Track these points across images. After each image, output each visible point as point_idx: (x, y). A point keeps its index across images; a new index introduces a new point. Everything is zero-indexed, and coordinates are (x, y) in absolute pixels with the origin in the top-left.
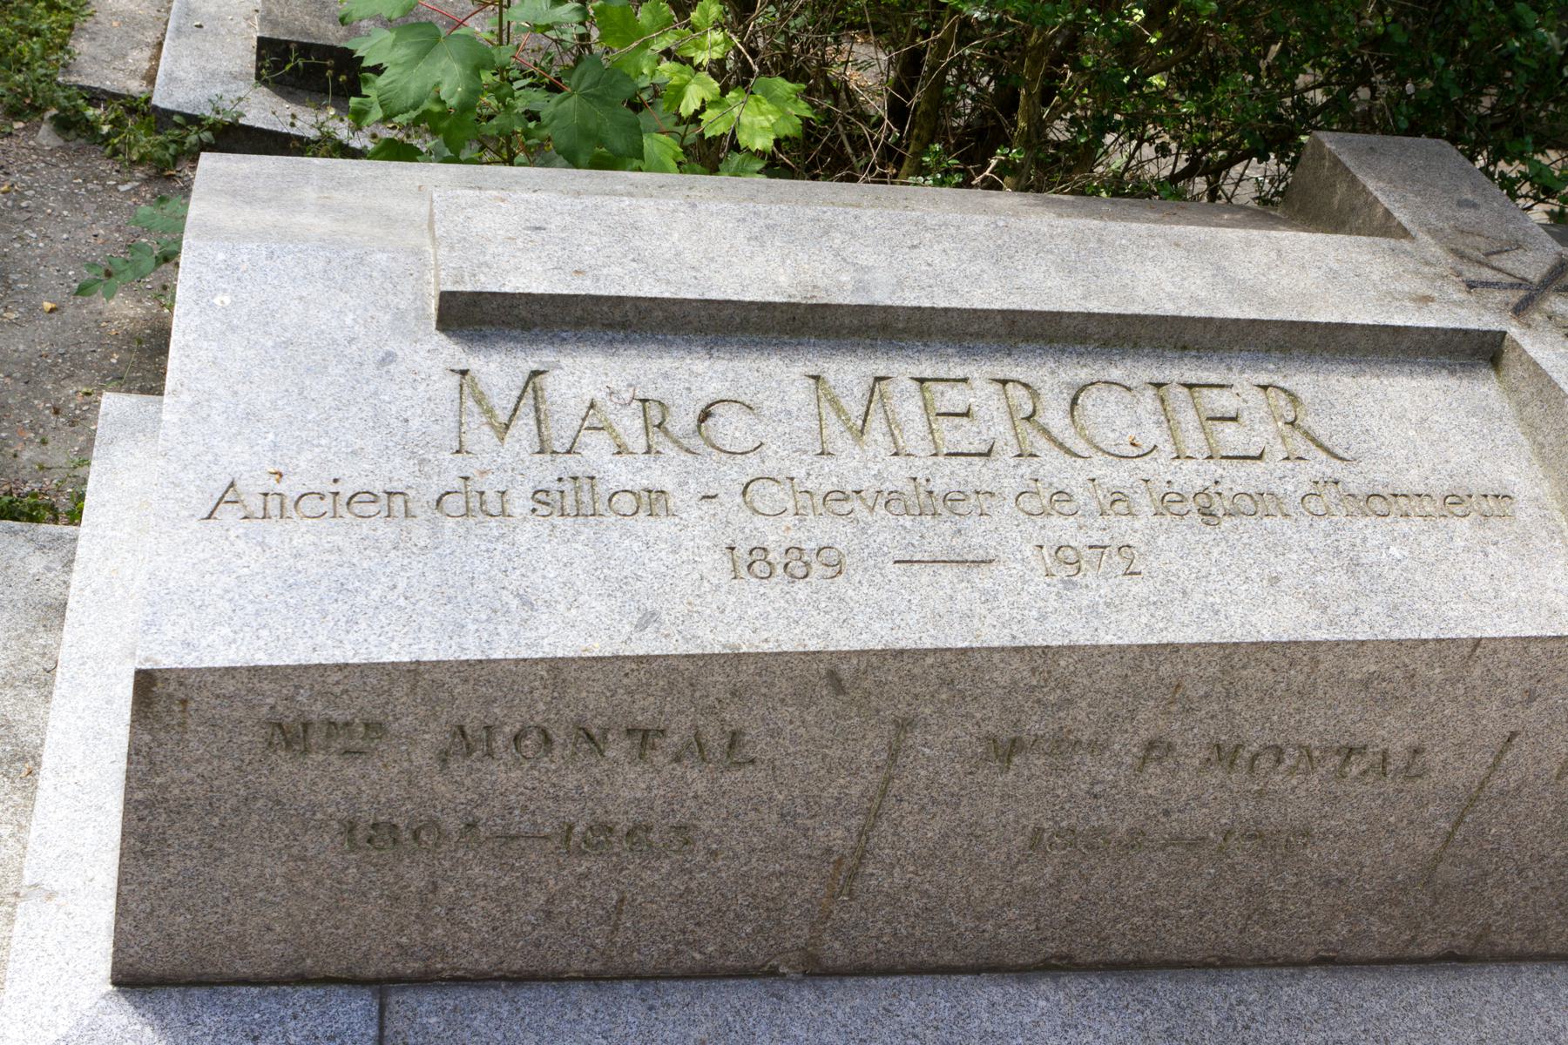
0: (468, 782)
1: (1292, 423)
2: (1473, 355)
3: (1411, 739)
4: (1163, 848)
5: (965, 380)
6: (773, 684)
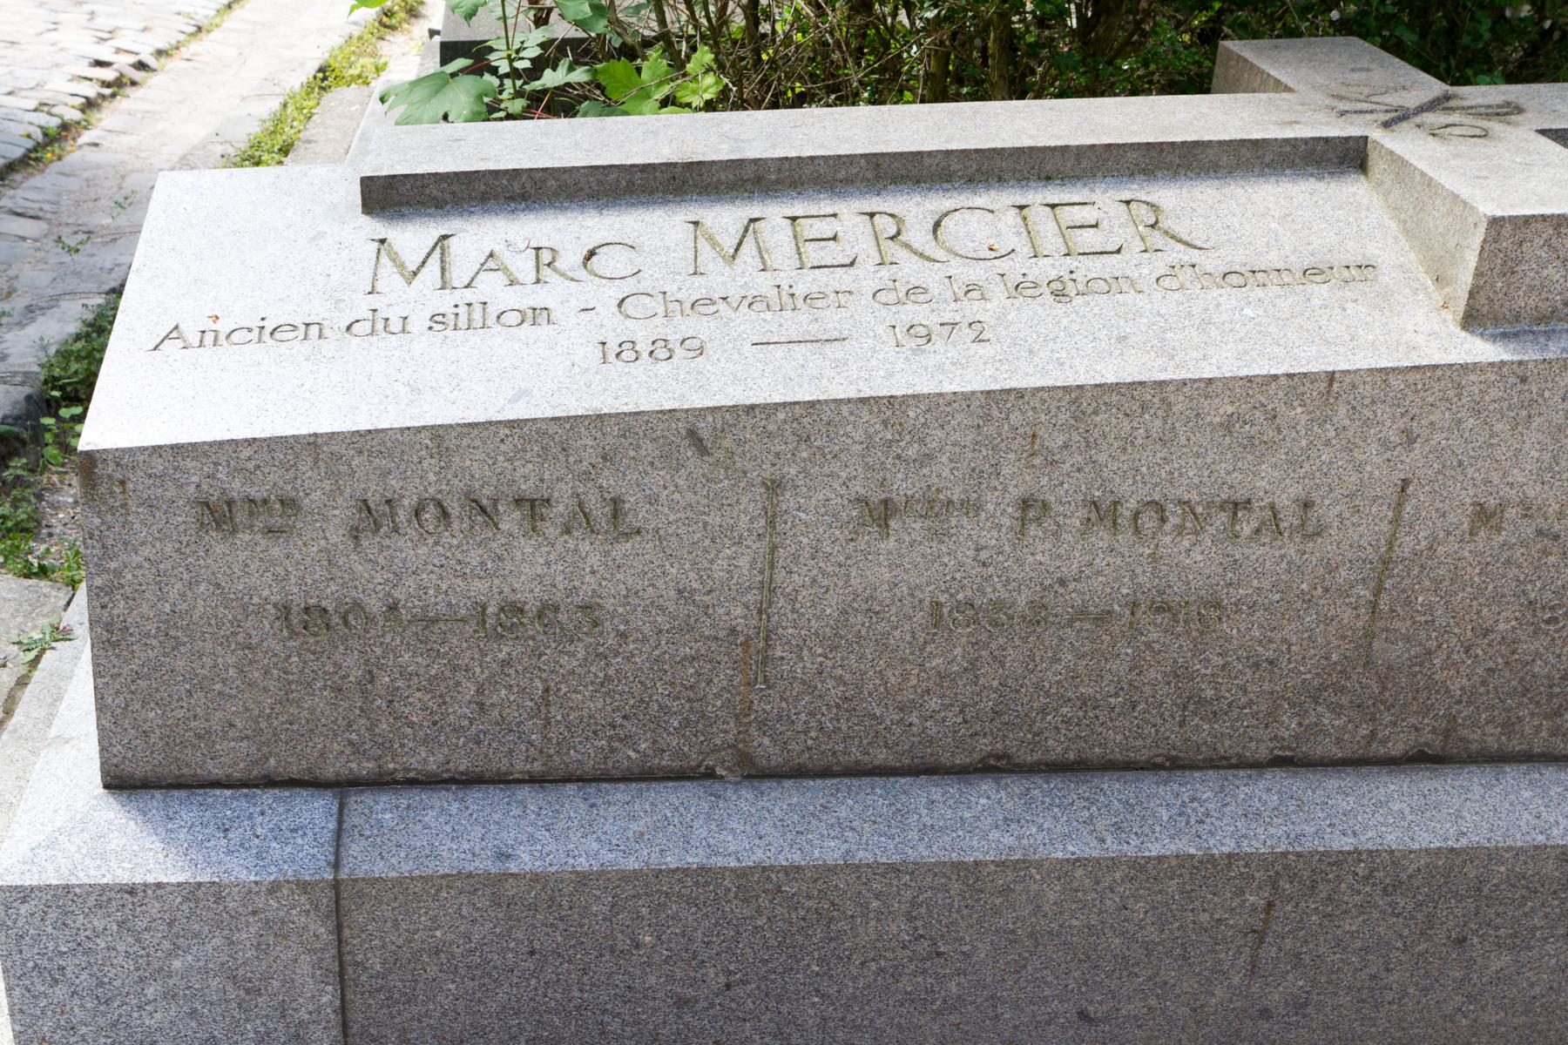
0: (381, 560)
1: (1152, 226)
2: (1341, 163)
3: (1295, 490)
4: (1070, 624)
5: (835, 215)
6: (639, 447)
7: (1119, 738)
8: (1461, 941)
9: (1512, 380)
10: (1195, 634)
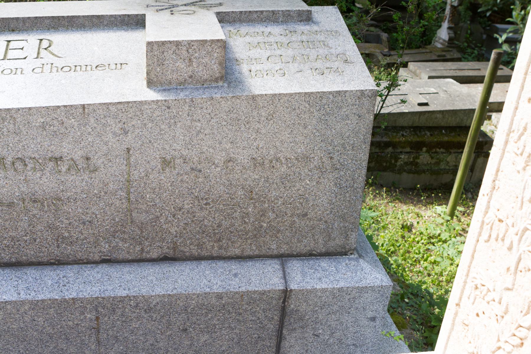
7: (32, 253)
8: (185, 330)
9: (164, 108)
10: (53, 211)
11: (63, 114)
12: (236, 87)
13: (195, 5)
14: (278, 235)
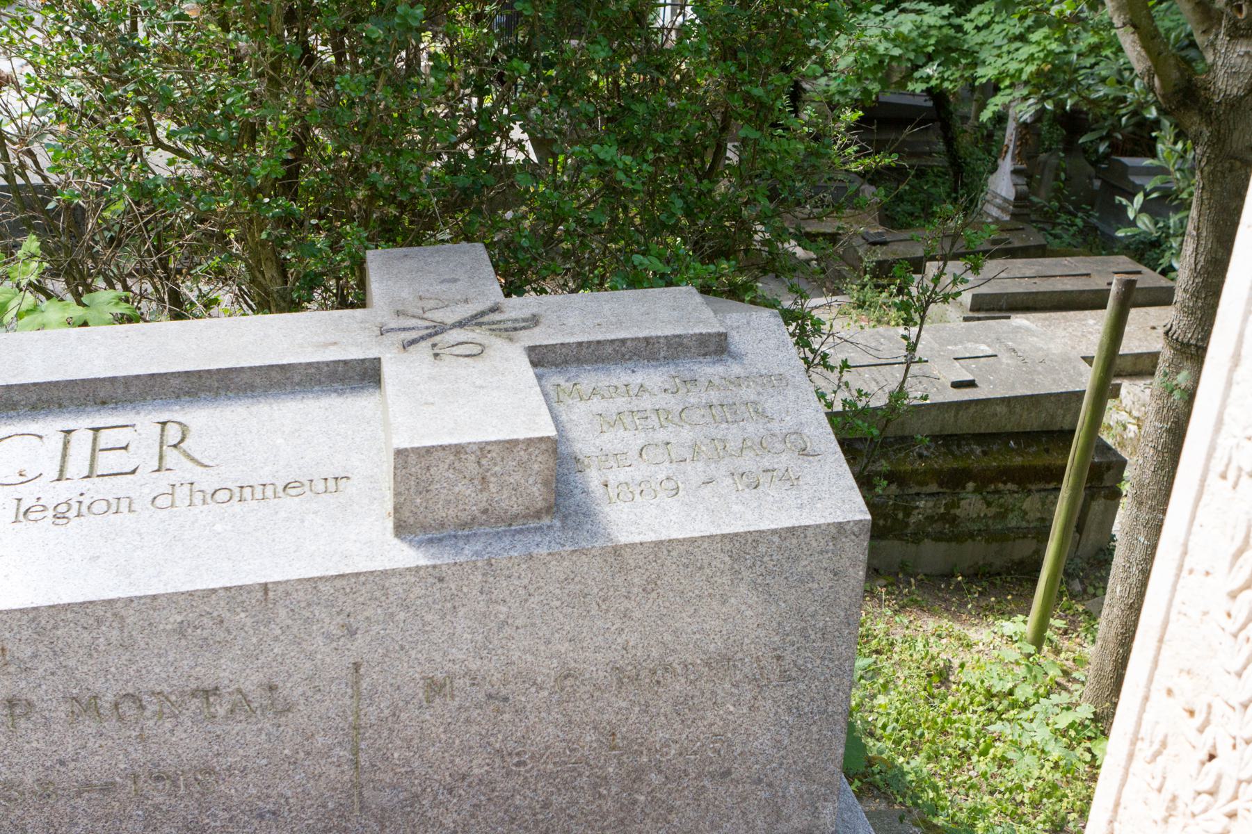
9: (431, 580)
10: (197, 795)
11: (222, 603)
12: (578, 527)
13: (480, 324)
14: (670, 818)
